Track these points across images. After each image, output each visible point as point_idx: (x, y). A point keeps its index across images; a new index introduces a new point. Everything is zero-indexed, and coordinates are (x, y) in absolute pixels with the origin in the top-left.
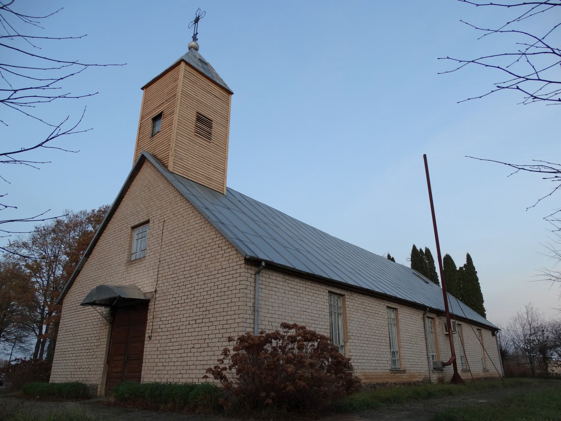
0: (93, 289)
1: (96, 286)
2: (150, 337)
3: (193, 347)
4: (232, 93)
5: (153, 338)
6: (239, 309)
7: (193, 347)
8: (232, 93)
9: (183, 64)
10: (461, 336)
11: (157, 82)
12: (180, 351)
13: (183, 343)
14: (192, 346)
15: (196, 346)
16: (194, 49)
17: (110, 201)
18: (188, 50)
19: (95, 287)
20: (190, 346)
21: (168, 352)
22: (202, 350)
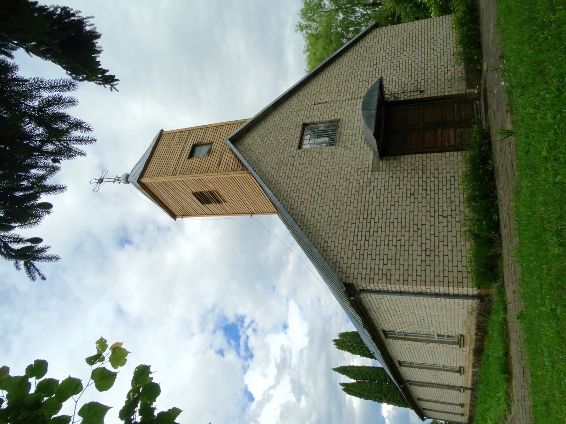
0: (363, 114)
1: (361, 110)
2: (421, 92)
3: (433, 49)
4: (162, 131)
5: (422, 89)
6: (453, 282)
7: (433, 49)
8: (162, 131)
9: (144, 180)
10: (467, 296)
11: (146, 173)
12: (436, 59)
13: (429, 58)
14: (432, 50)
15: (432, 47)
16: (127, 180)
17: (251, 114)
18: (131, 184)
19: (361, 112)
20: (432, 52)
21: (436, 70)
22: (435, 42)
